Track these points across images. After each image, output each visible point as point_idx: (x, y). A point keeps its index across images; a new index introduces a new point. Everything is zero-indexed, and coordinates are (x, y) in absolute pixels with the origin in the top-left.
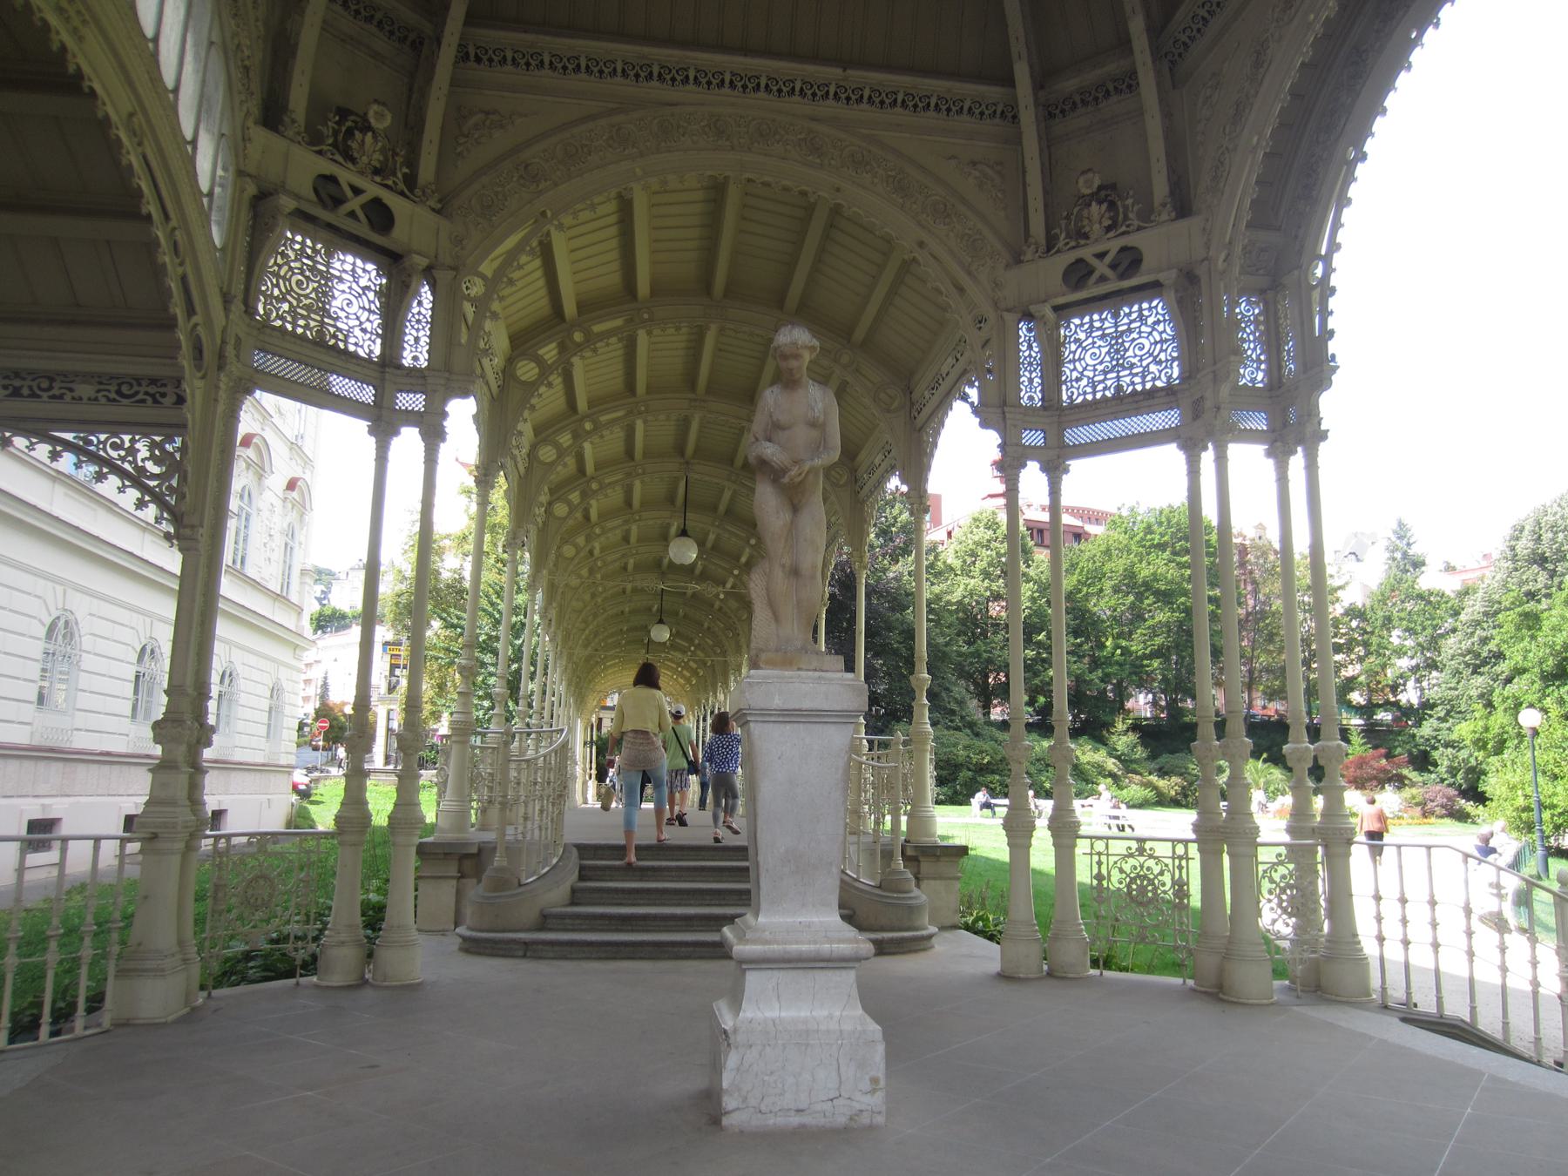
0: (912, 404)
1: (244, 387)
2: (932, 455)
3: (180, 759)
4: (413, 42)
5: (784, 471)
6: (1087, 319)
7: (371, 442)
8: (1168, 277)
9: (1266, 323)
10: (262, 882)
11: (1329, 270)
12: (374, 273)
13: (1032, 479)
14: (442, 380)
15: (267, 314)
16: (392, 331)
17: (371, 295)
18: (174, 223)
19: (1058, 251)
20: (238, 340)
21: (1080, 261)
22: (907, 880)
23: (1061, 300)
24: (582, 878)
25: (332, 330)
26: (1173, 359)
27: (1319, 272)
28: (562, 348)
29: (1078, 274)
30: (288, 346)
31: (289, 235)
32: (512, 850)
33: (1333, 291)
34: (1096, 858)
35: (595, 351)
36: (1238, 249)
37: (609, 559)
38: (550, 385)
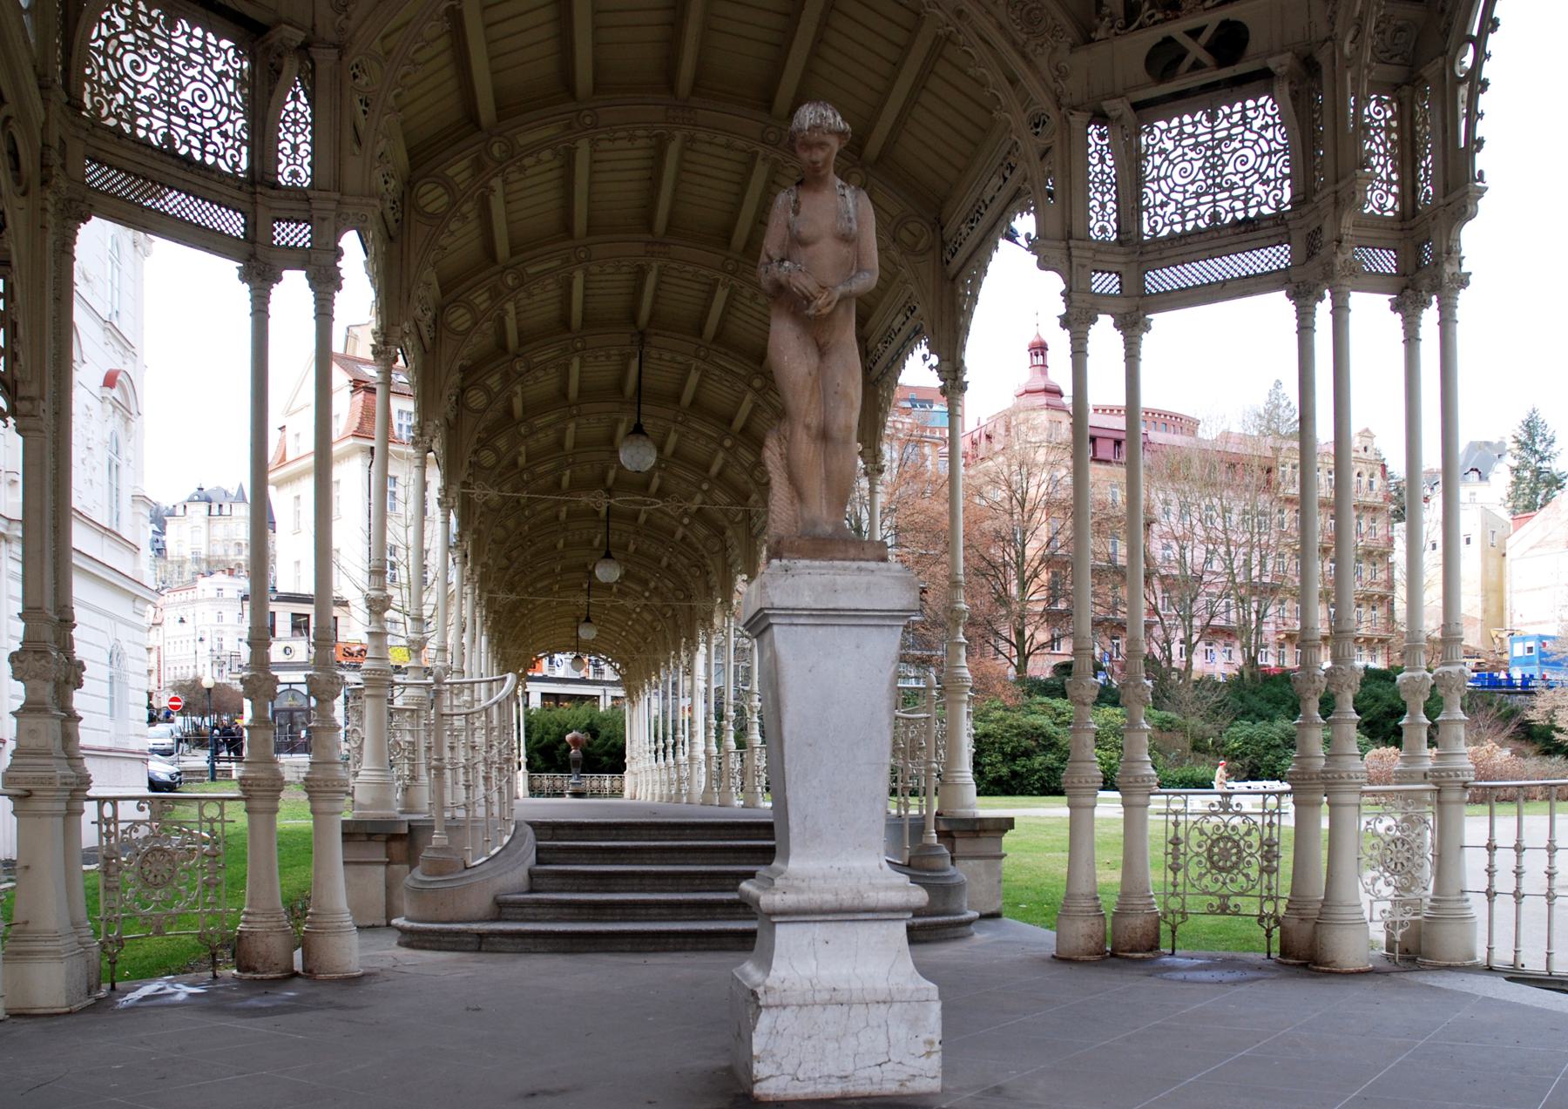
0: (944, 244)
1: (79, 209)
2: (969, 314)
3: (48, 700)
5: (809, 299)
6: (1175, 122)
9: (1399, 130)
10: (158, 854)
11: (1481, 56)
12: (231, 53)
14: (323, 207)
15: (97, 108)
17: (230, 85)
19: (1140, 26)
20: (62, 141)
21: (1169, 40)
22: (942, 856)
24: (539, 862)
25: (183, 133)
26: (1285, 177)
27: (1468, 60)
28: (478, 166)
29: (1164, 60)
30: (123, 153)
32: (454, 827)
33: (1485, 85)
36: (1370, 26)
37: (540, 469)
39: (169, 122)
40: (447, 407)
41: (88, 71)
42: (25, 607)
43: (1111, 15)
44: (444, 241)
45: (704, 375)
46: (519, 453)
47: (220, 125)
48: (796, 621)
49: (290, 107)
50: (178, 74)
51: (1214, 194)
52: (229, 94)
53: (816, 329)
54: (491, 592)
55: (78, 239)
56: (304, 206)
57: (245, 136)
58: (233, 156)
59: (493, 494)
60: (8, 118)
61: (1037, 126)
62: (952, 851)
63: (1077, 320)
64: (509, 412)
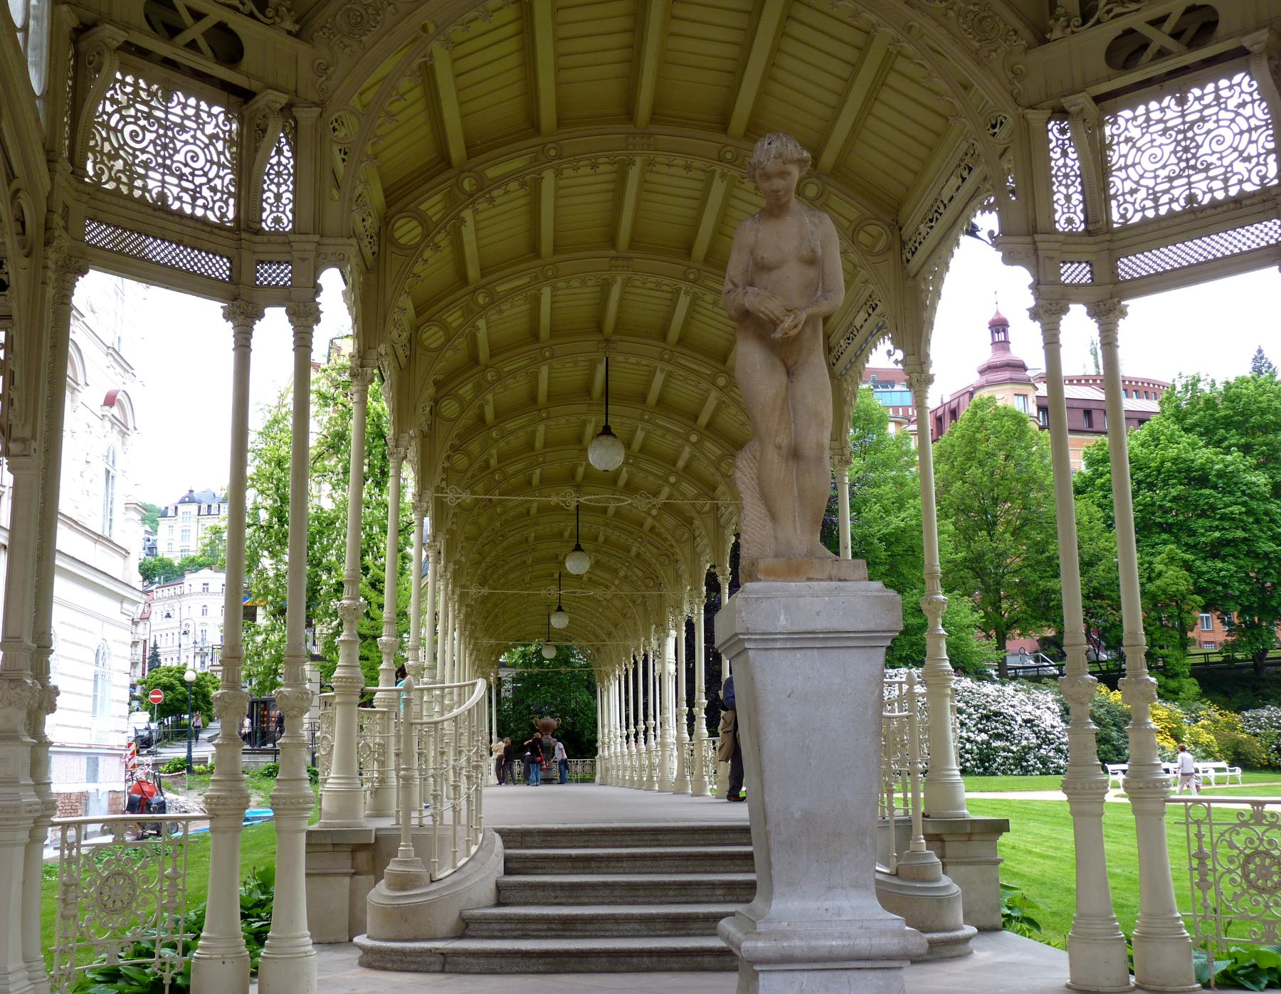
0: (903, 244)
2: (934, 308)
5: (774, 324)
7: (228, 329)
8: (1256, 40)
12: (222, 117)
13: (1078, 325)
14: (309, 246)
16: (247, 186)
17: (220, 145)
19: (1099, 22)
21: (1130, 32)
23: (1105, 88)
24: (508, 872)
26: (1269, 152)
29: (1127, 51)
31: (118, 76)
34: (1194, 829)
35: (492, 200)
37: (511, 470)
38: (437, 247)
39: (163, 182)
40: (422, 418)
41: (234, 149)
43: (1066, 14)
44: (418, 268)
45: (670, 375)
46: (492, 456)
47: (210, 180)
48: (770, 645)
49: (274, 161)
50: (172, 139)
51: (1189, 176)
52: (219, 153)
53: (785, 352)
54: (463, 587)
55: (76, 291)
56: (286, 248)
57: (232, 189)
58: (221, 208)
59: (467, 497)
60: (18, 191)
61: (994, 126)
62: (942, 857)
63: (1049, 309)
64: (481, 419)
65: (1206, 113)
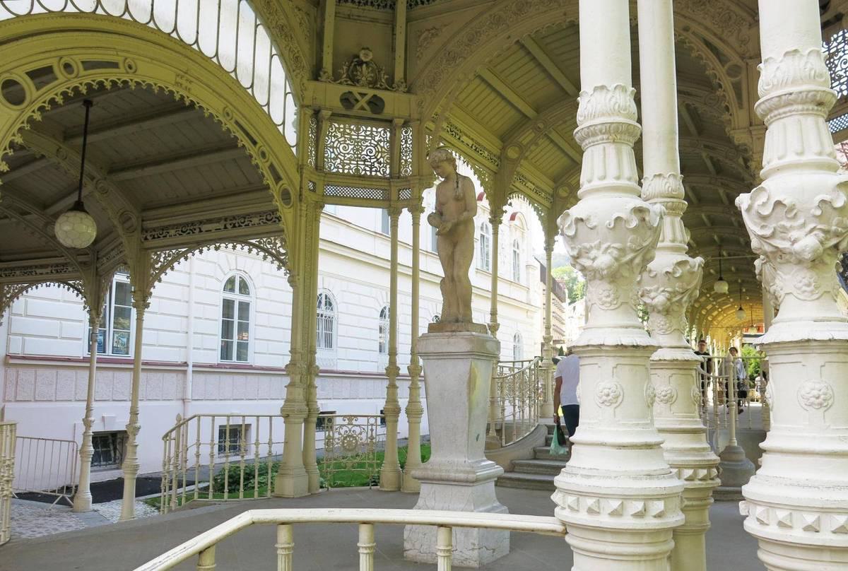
4: (391, 5)
18: (260, 144)
25: (363, 167)
34: (370, 427)
41: (326, 155)
42: (292, 349)
57: (388, 161)
65: (839, 47)
